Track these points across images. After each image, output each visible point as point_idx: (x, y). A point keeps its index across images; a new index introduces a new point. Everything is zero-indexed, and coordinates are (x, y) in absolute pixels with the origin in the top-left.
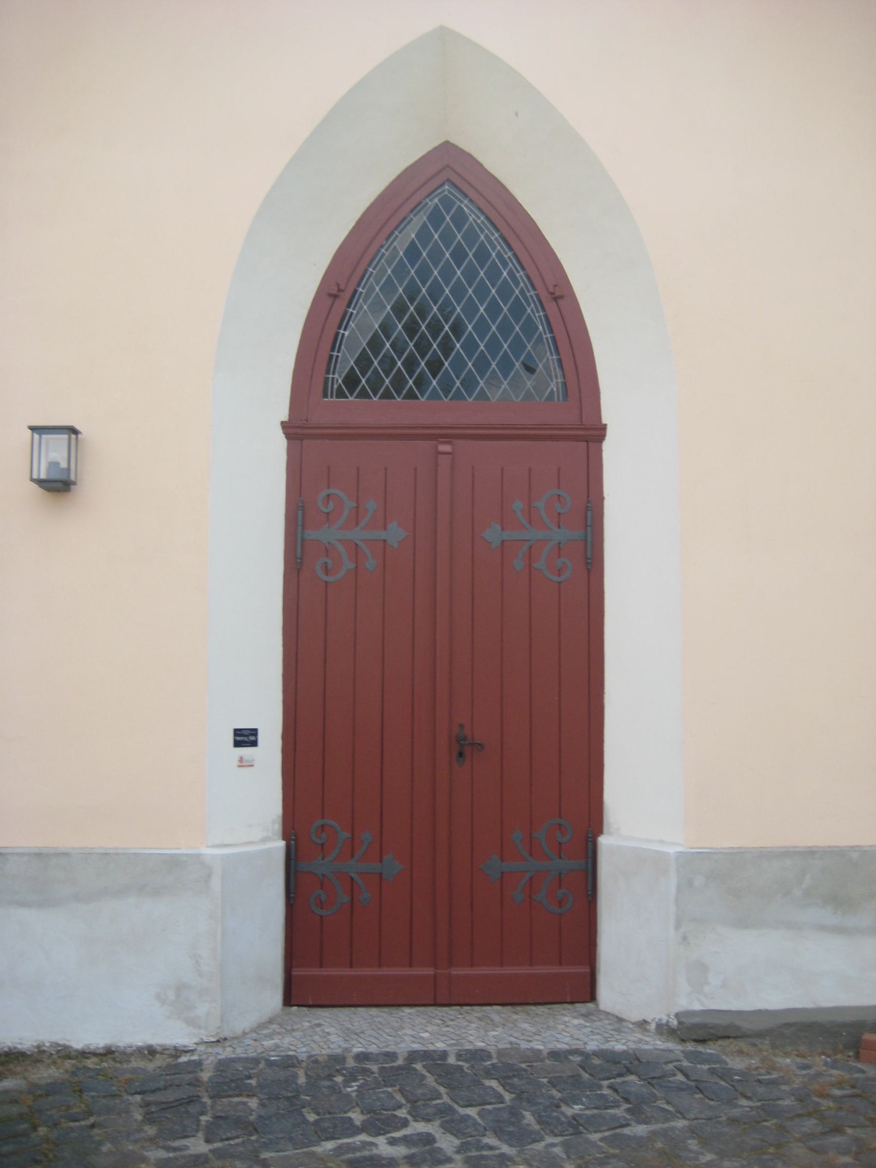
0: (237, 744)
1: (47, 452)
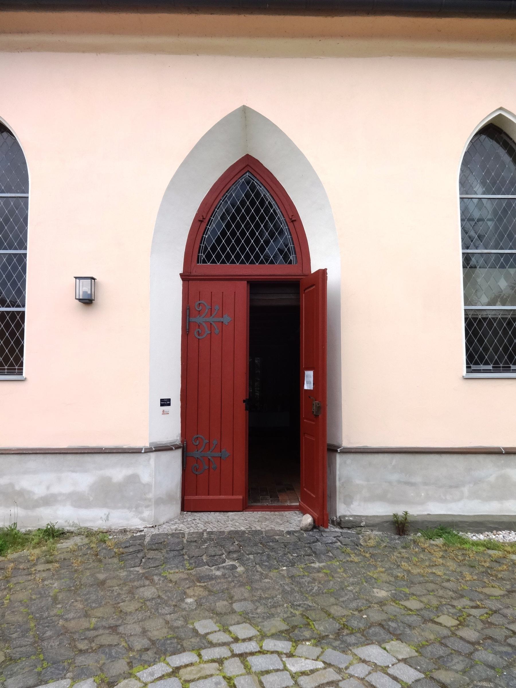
0: (162, 405)
1: (83, 287)
